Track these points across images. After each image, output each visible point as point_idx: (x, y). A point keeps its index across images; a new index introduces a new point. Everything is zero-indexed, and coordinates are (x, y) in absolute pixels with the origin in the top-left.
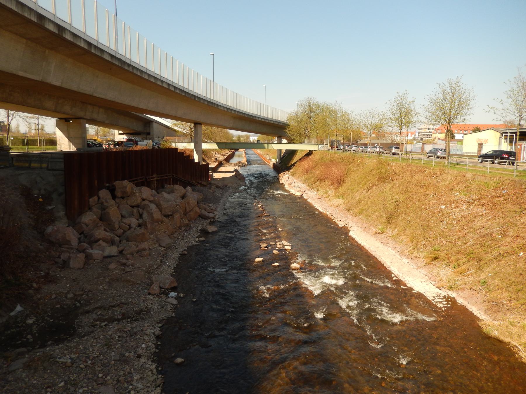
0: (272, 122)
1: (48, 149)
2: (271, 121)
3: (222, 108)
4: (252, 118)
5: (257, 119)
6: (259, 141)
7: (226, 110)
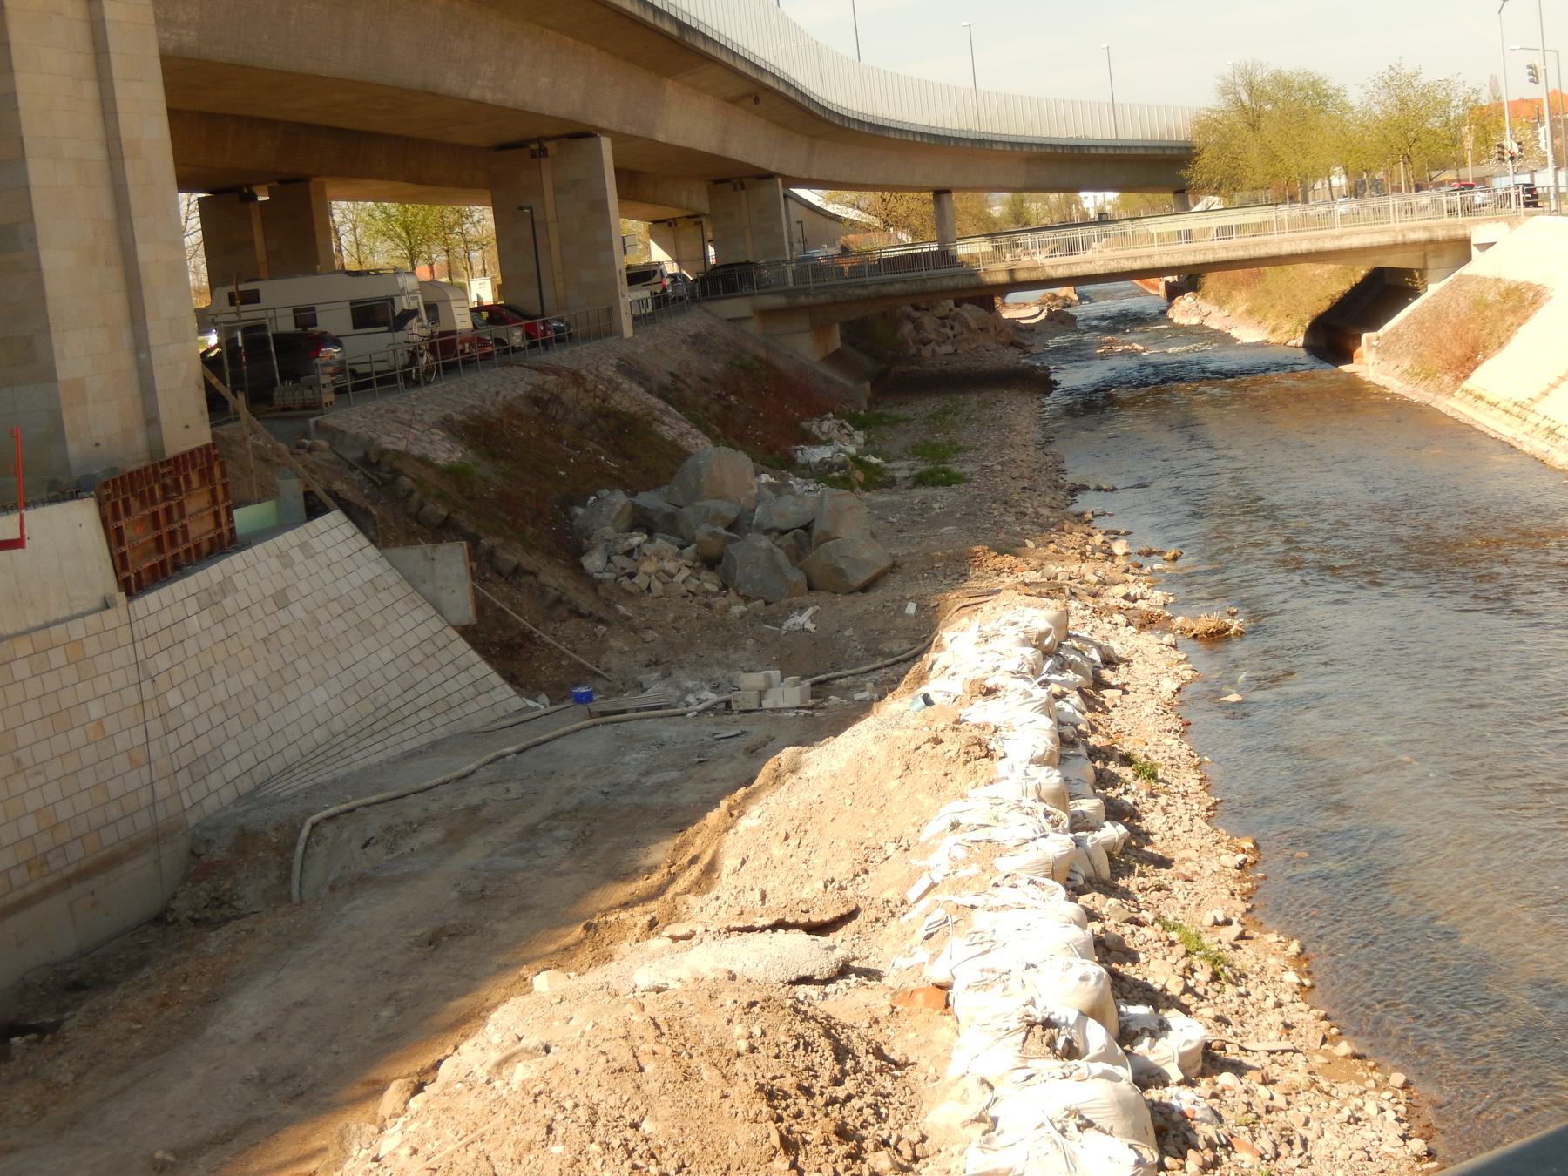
0: (1142, 152)
1: (1259, 228)
2: (1136, 148)
3: (1000, 147)
4: (1077, 152)
5: (1093, 151)
6: (1104, 217)
7: (1009, 148)
